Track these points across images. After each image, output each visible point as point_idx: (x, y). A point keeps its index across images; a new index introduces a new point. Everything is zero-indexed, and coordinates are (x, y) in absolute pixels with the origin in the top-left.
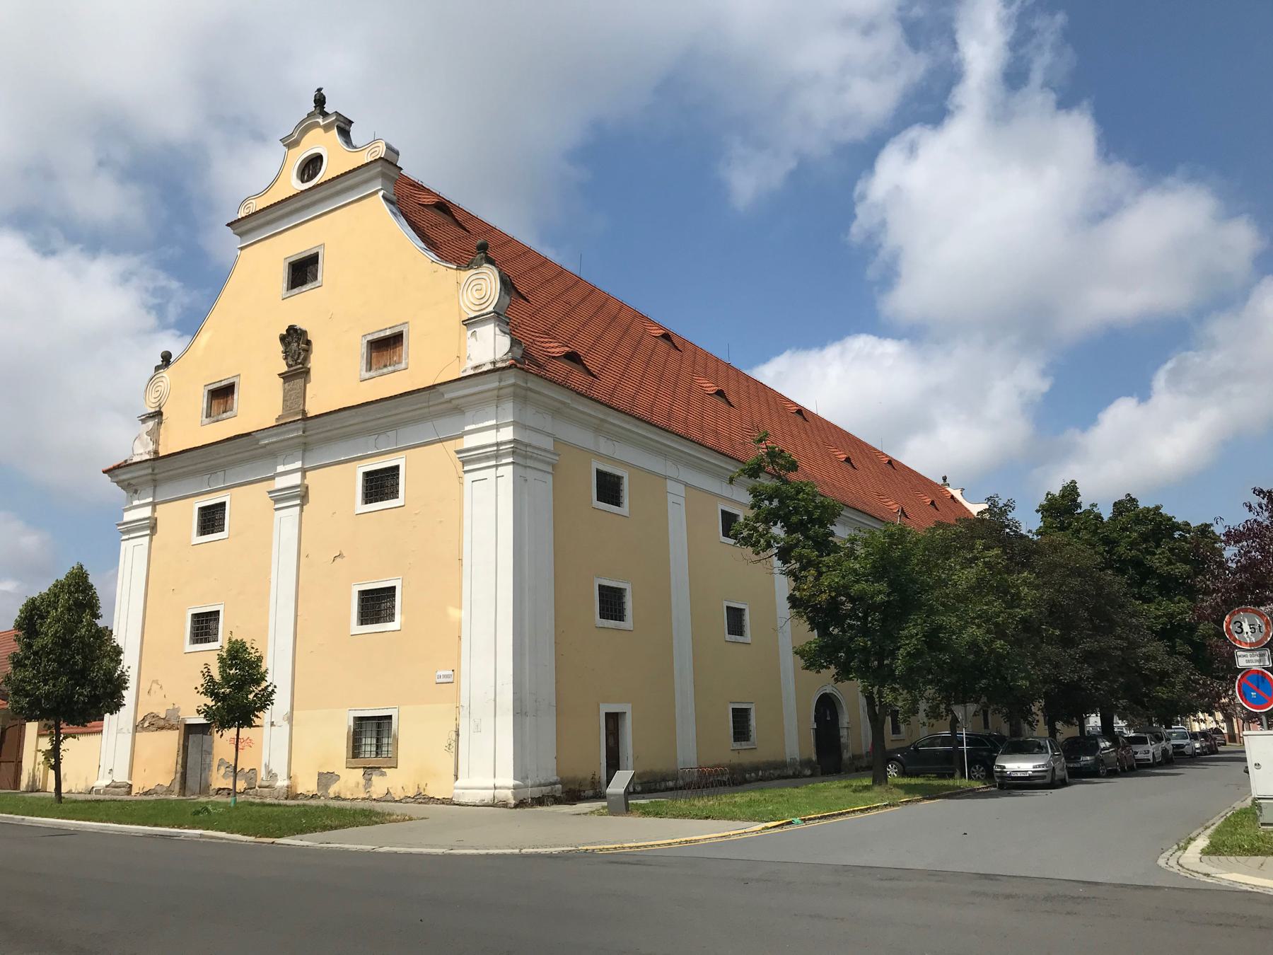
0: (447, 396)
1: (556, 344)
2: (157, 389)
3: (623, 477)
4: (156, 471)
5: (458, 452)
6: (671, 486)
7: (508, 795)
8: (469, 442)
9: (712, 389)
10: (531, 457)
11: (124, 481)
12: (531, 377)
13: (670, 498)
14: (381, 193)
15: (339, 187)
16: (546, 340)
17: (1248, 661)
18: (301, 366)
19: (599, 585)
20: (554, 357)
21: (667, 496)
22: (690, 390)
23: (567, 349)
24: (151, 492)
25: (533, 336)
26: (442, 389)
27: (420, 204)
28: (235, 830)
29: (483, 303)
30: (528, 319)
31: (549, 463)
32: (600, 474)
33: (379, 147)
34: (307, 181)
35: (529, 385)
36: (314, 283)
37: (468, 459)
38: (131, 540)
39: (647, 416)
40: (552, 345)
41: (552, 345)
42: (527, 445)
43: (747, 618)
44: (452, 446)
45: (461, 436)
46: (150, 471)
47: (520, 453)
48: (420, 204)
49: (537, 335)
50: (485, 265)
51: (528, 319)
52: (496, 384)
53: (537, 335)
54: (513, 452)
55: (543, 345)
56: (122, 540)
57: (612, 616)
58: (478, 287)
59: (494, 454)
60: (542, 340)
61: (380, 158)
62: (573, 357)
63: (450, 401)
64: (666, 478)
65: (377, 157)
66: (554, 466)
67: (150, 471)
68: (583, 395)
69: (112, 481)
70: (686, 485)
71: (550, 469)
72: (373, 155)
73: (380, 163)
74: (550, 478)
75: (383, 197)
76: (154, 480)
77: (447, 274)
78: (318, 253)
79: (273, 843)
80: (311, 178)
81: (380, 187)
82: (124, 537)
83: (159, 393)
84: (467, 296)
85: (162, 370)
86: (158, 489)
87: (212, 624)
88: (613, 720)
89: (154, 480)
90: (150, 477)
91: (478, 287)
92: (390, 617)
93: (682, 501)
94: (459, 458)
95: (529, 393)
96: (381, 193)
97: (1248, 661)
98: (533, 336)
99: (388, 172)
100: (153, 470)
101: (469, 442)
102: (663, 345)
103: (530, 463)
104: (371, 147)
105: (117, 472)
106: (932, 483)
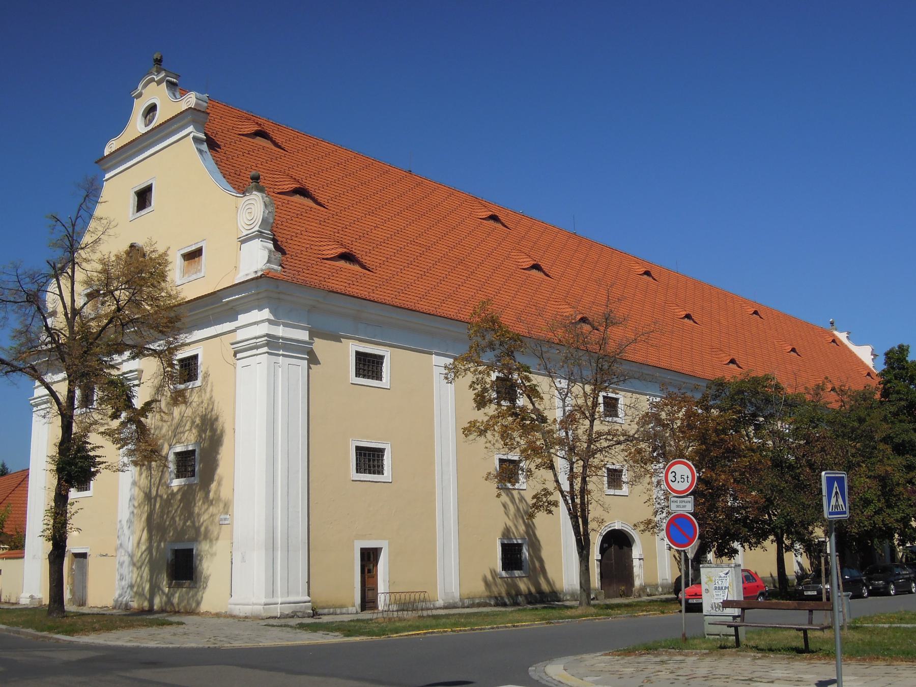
5: (232, 344)
17: (678, 506)
31: (45, 403)
34: (148, 125)
36: (149, 208)
48: (240, 135)
50: (254, 193)
61: (191, 108)
72: (189, 104)
73: (190, 110)
80: (151, 122)
88: (369, 557)
91: (249, 211)
92: (87, 489)
97: (678, 506)
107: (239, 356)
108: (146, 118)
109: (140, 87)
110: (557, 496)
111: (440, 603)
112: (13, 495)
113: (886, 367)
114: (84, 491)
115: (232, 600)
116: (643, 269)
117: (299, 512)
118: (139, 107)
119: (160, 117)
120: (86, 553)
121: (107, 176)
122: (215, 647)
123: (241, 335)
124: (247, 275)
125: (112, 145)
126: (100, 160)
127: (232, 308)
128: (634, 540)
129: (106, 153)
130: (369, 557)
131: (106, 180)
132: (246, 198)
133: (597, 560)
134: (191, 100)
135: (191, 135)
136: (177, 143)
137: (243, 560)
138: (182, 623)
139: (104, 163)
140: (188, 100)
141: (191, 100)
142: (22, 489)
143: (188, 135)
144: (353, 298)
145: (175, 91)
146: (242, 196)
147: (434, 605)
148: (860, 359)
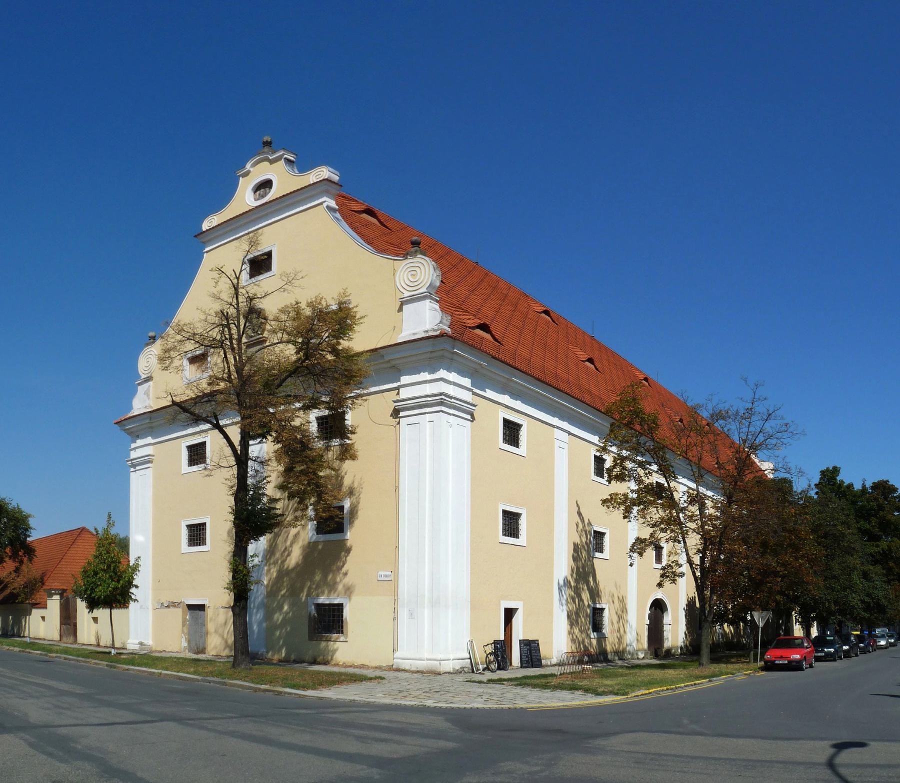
0: (387, 358)
9: (584, 357)
13: (557, 444)
16: (461, 313)
18: (261, 336)
19: (503, 510)
21: (569, 441)
23: (479, 321)
25: (451, 310)
27: (352, 211)
28: (283, 694)
34: (258, 199)
36: (269, 273)
39: (541, 376)
40: (466, 317)
41: (466, 317)
43: (607, 539)
48: (352, 211)
49: (454, 309)
52: (430, 349)
53: (454, 309)
55: (459, 317)
57: (511, 534)
58: (414, 273)
59: (237, 423)
60: (458, 313)
61: (324, 180)
62: (484, 327)
63: (389, 361)
65: (321, 179)
71: (469, 417)
72: (318, 177)
77: (381, 263)
78: (271, 251)
79: (8, 649)
80: (263, 197)
88: (509, 613)
91: (414, 273)
93: (565, 446)
98: (451, 310)
104: (315, 172)
106: (238, 468)
108: (255, 192)
110: (686, 568)
111: (554, 661)
112: (70, 552)
113: (838, 478)
114: (197, 545)
115: (397, 654)
116: (643, 376)
119: (273, 194)
121: (207, 249)
122: (503, 708)
123: (405, 393)
124: (414, 334)
126: (199, 235)
127: (394, 366)
128: (667, 609)
129: (205, 226)
130: (509, 613)
131: (207, 252)
133: (647, 625)
135: (325, 205)
136: (305, 212)
137: (411, 615)
139: (203, 238)
140: (319, 173)
141: (324, 172)
142: (76, 546)
143: (321, 204)
145: (293, 167)
147: (551, 662)
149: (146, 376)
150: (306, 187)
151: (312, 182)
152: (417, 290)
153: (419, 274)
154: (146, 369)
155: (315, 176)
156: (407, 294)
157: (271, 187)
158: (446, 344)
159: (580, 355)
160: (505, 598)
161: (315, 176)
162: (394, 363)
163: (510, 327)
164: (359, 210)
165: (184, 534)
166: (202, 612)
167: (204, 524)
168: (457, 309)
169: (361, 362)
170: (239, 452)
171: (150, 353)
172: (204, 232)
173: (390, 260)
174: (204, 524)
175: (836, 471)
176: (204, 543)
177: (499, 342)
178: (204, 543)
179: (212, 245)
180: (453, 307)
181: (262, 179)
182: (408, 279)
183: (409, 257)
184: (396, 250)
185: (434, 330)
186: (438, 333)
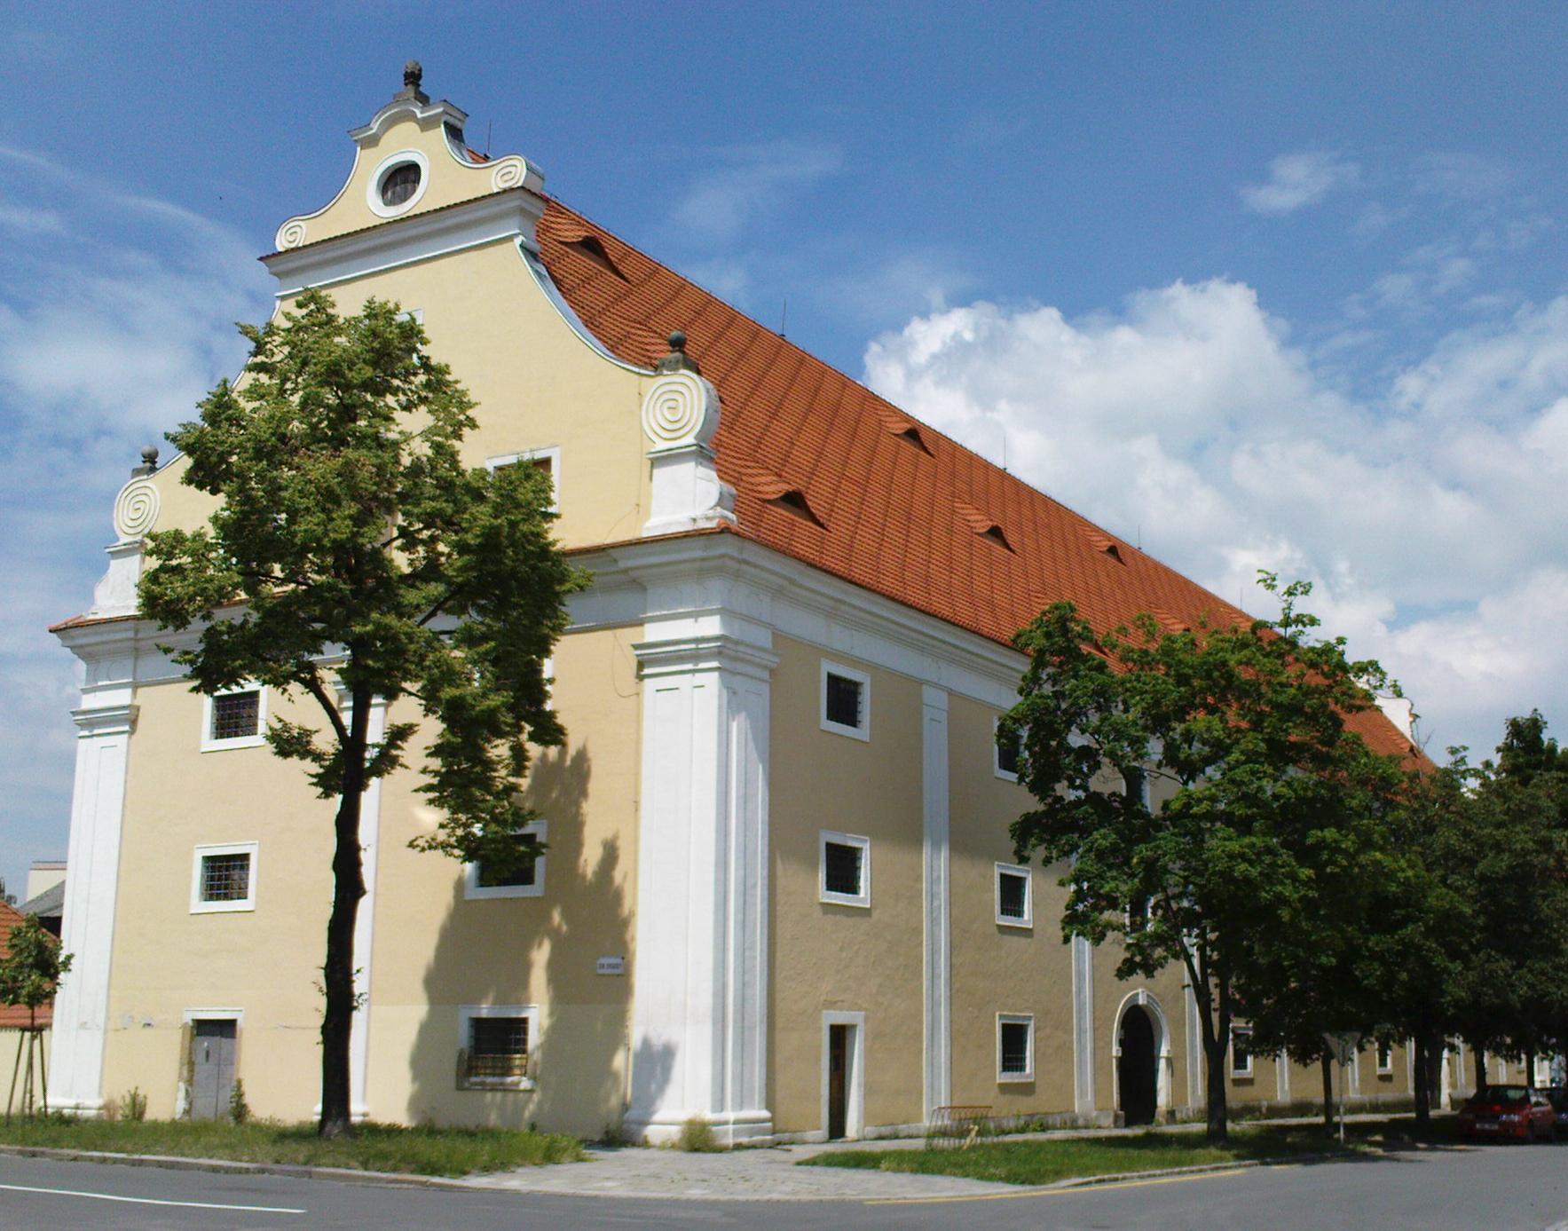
0: (622, 564)
1: (769, 479)
2: (137, 506)
3: (862, 684)
4: (140, 636)
5: (636, 647)
6: (929, 694)
7: (1489, 1080)
8: (654, 632)
9: (983, 527)
10: (742, 660)
11: (82, 646)
12: (748, 544)
14: (518, 241)
15: (449, 222)
16: (755, 471)
20: (769, 501)
22: (950, 532)
24: (130, 667)
26: (615, 553)
29: (680, 428)
30: (633, 331)
32: (834, 681)
33: (515, 166)
35: (745, 556)
37: (647, 661)
38: (95, 738)
42: (737, 643)
44: (629, 636)
45: (640, 623)
46: (131, 634)
47: (727, 654)
48: (561, 242)
51: (633, 331)
54: (720, 653)
56: (80, 737)
63: (626, 571)
64: (921, 682)
66: (772, 672)
67: (131, 634)
68: (815, 567)
69: (63, 646)
70: (951, 693)
72: (506, 178)
74: (766, 688)
75: (521, 246)
76: (136, 649)
77: (616, 376)
81: (518, 231)
82: (82, 733)
83: (140, 512)
84: (655, 416)
85: (145, 477)
86: (141, 663)
87: (236, 874)
89: (136, 649)
90: (132, 644)
94: (638, 656)
95: (744, 567)
96: (518, 241)
99: (528, 207)
100: (136, 633)
101: (654, 632)
102: (908, 448)
103: (740, 667)
105: (73, 632)
107: (647, 671)
109: (375, 127)
116: (1105, 543)
117: (755, 958)
118: (371, 166)
120: (1005, 1027)
125: (298, 229)
132: (660, 380)
134: (511, 171)
138: (790, 1150)
144: (631, 548)
146: (652, 374)
148: (1390, 722)
149: (130, 539)
150: (484, 197)
151: (496, 190)
152: (679, 438)
153: (681, 408)
154: (131, 523)
155: (500, 175)
156: (662, 445)
157: (417, 180)
158: (728, 547)
159: (977, 521)
160: (831, 1005)
161: (500, 175)
162: (632, 574)
163: (845, 485)
164: (575, 240)
165: (197, 872)
166: (229, 1040)
167: (245, 857)
168: (748, 464)
169: (575, 568)
170: (349, 732)
171: (143, 491)
172: (280, 253)
173: (632, 374)
174: (245, 857)
175: (1535, 725)
176: (242, 895)
177: (822, 526)
178: (242, 895)
179: (733, 1094)
180: (740, 459)
181: (397, 161)
182: (663, 415)
183: (665, 372)
184: (639, 336)
185: (708, 519)
186: (713, 524)
